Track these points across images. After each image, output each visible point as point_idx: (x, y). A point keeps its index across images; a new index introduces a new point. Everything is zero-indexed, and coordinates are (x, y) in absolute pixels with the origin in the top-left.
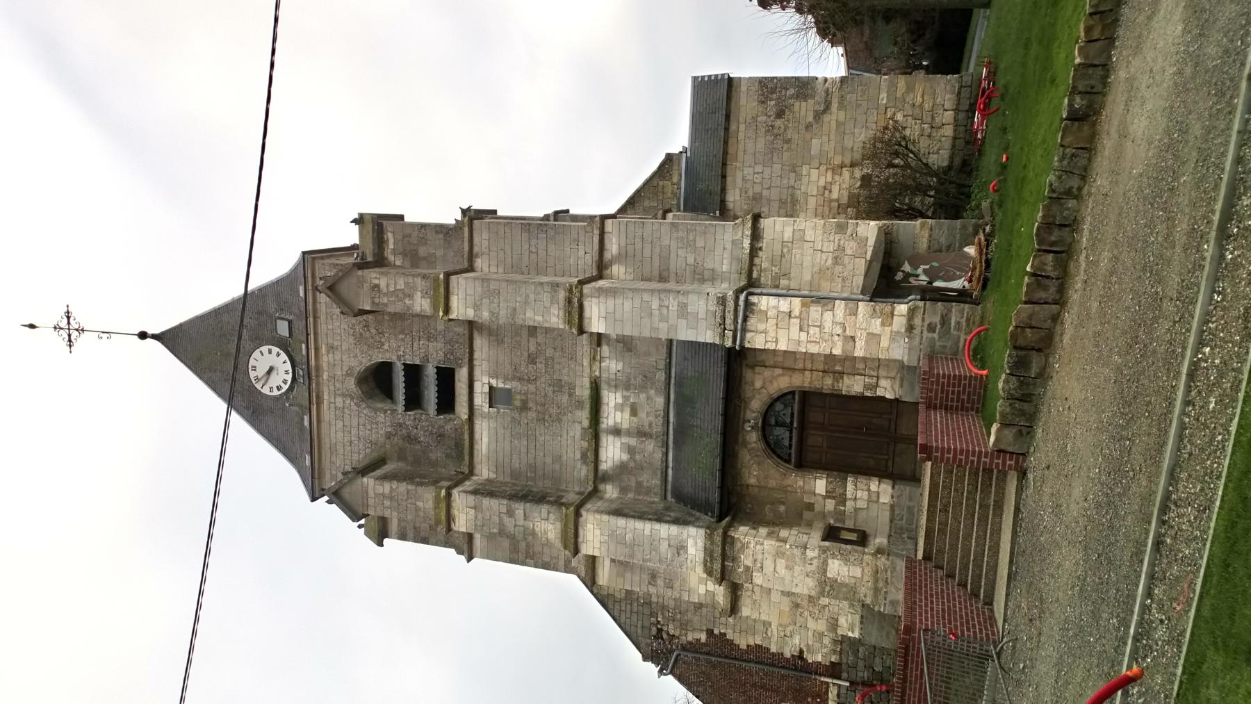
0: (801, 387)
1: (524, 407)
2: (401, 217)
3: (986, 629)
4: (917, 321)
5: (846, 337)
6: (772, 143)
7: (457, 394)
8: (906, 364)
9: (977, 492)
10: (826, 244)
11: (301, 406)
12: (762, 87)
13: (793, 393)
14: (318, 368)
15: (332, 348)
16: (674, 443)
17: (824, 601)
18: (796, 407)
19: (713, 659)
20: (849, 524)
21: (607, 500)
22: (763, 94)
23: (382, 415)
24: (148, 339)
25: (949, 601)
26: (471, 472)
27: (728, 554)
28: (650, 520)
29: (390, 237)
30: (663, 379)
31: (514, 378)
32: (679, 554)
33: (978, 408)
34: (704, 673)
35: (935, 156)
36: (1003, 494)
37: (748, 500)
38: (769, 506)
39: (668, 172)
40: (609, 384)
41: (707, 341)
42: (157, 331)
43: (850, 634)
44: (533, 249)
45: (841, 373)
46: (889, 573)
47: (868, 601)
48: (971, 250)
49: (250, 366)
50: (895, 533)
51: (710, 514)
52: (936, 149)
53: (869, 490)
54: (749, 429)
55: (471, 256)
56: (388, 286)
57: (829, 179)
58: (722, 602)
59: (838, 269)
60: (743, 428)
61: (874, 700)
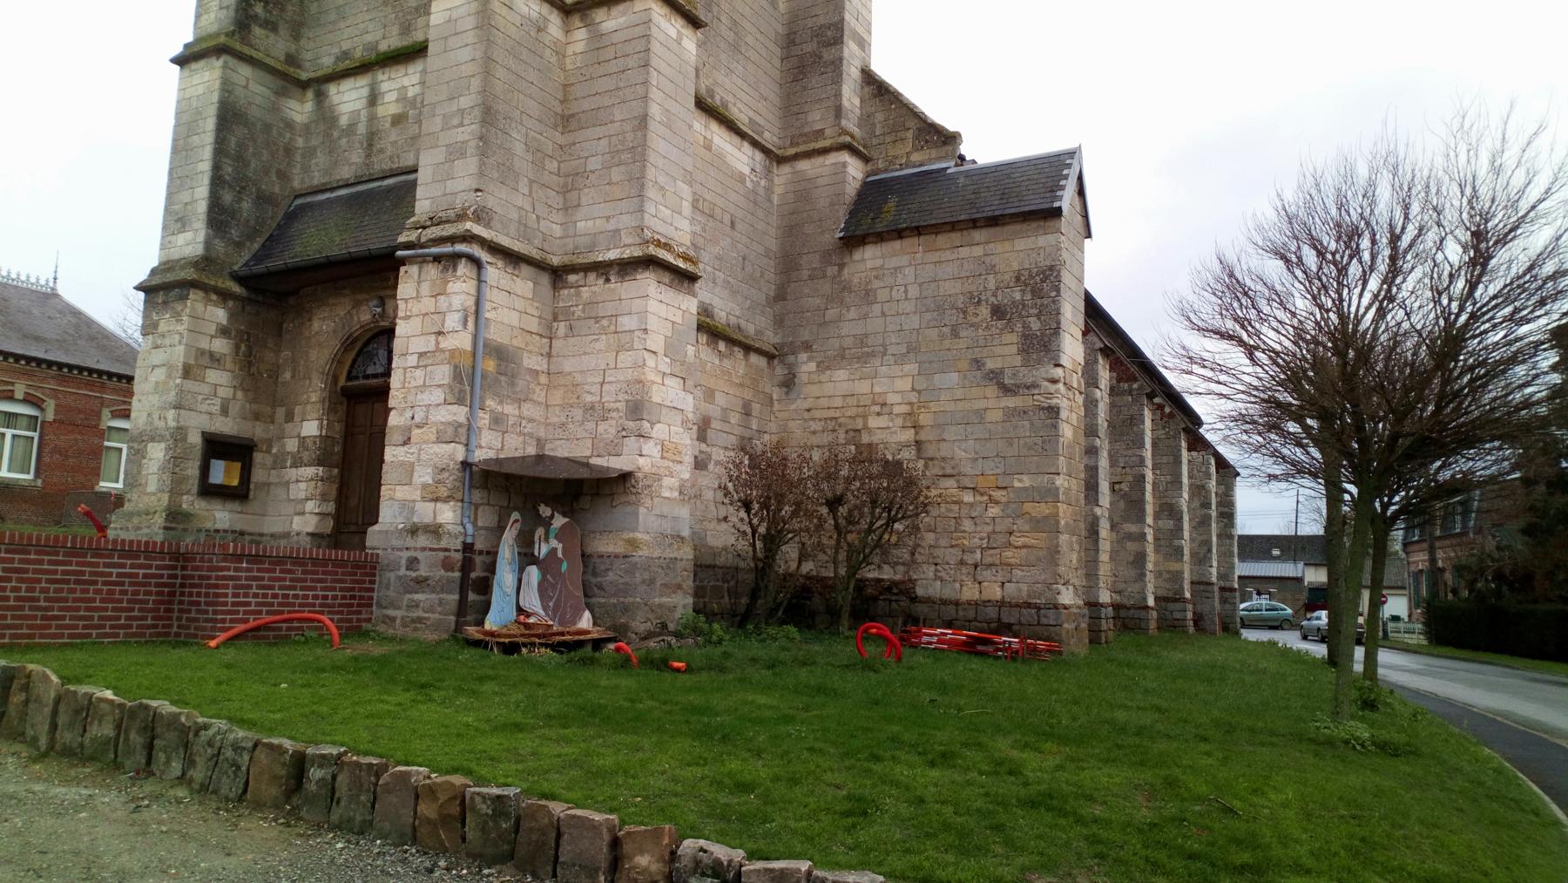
5: (409, 429)
6: (953, 307)
12: (1043, 273)
22: (1031, 277)
35: (931, 575)
39: (927, 141)
48: (585, 621)
52: (943, 574)
59: (578, 413)
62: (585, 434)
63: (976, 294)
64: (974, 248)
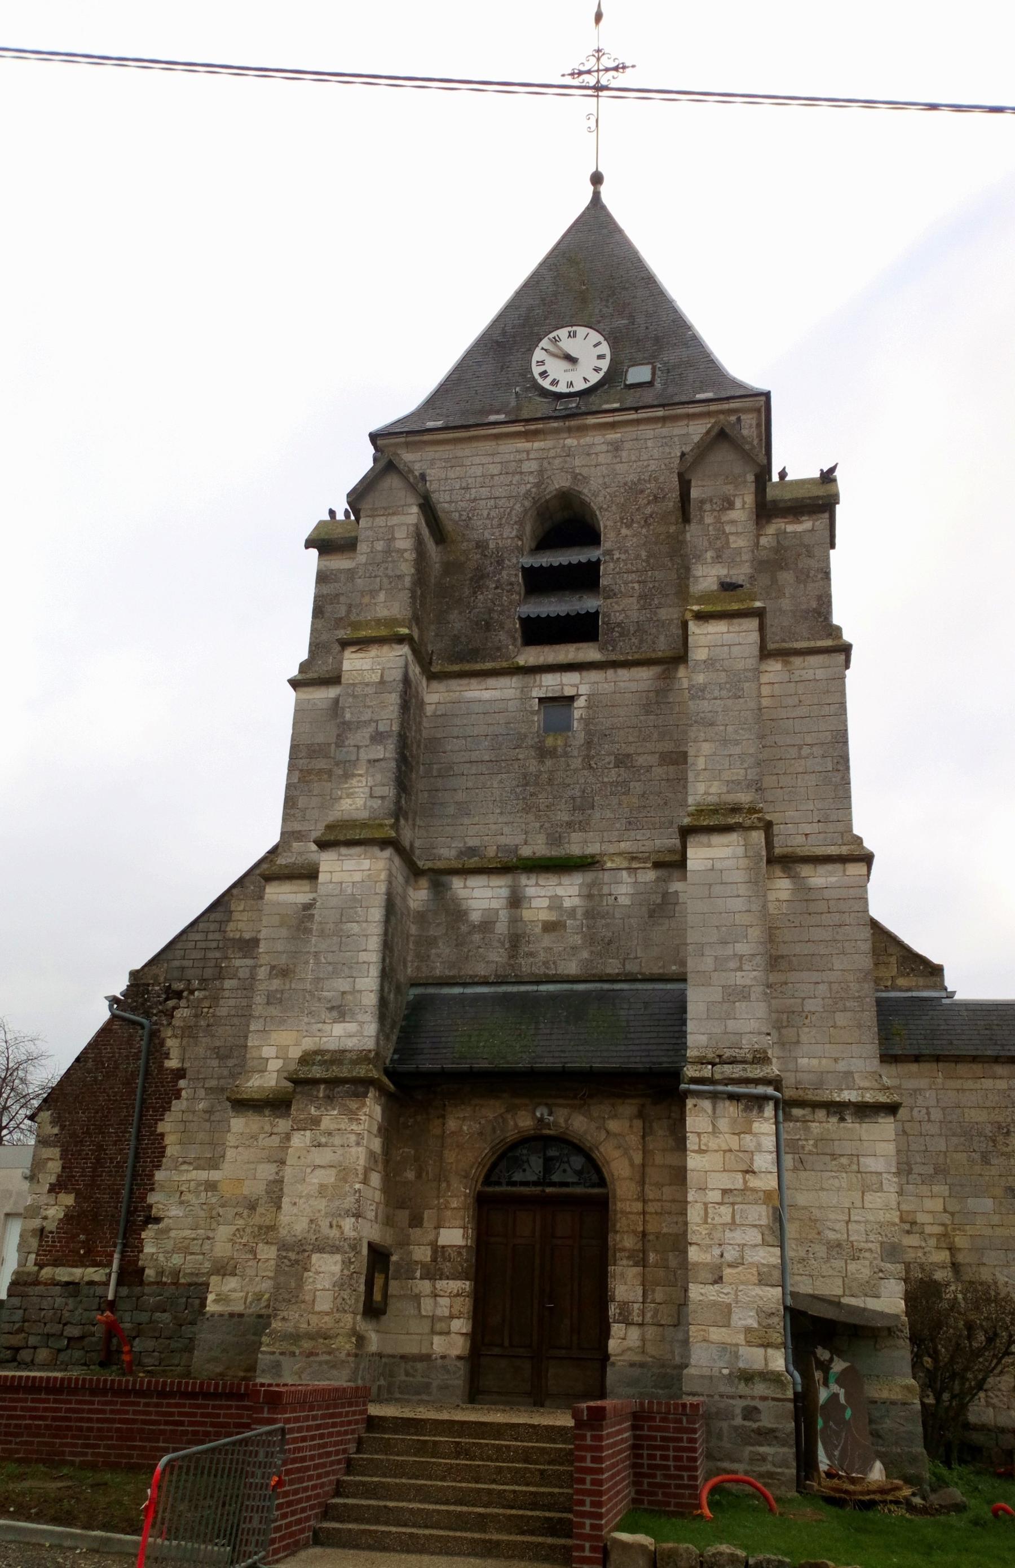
0: (615, 1197)
1: (543, 753)
2: (833, 546)
3: (282, 1538)
4: (760, 1389)
5: (720, 1267)
6: (980, 1134)
7: (557, 647)
8: (685, 1371)
9: (504, 1507)
10: (861, 1228)
11: (519, 408)
13: (602, 1182)
14: (583, 429)
15: (617, 449)
16: (505, 994)
17: (268, 1253)
18: (579, 1190)
19: (139, 1081)
20: (394, 1287)
21: (405, 890)
23: (514, 533)
24: (591, 188)
25: (316, 1467)
26: (432, 677)
27: (337, 1090)
28: (384, 960)
29: (806, 525)
30: (609, 971)
31: (589, 733)
32: (332, 1009)
33: (642, 1502)
34: (116, 1068)
36: (512, 1557)
37: (419, 1118)
38: (413, 1152)
40: (591, 885)
41: (688, 1036)
42: (606, 198)
43: (211, 1297)
44: (806, 750)
45: (643, 1263)
46: (327, 1357)
47: (276, 1324)
48: (877, 1473)
49: (575, 328)
50: (386, 1364)
51: (396, 1057)
52: (995, 1401)
53: (452, 1317)
54: (538, 1114)
55: (785, 654)
56: (733, 522)
57: (928, 1229)
58: (250, 1084)
59: (821, 1251)
60: (539, 1104)
61: (87, 1340)
62: (831, 1272)
63: (1004, 1125)
64: (998, 1081)
